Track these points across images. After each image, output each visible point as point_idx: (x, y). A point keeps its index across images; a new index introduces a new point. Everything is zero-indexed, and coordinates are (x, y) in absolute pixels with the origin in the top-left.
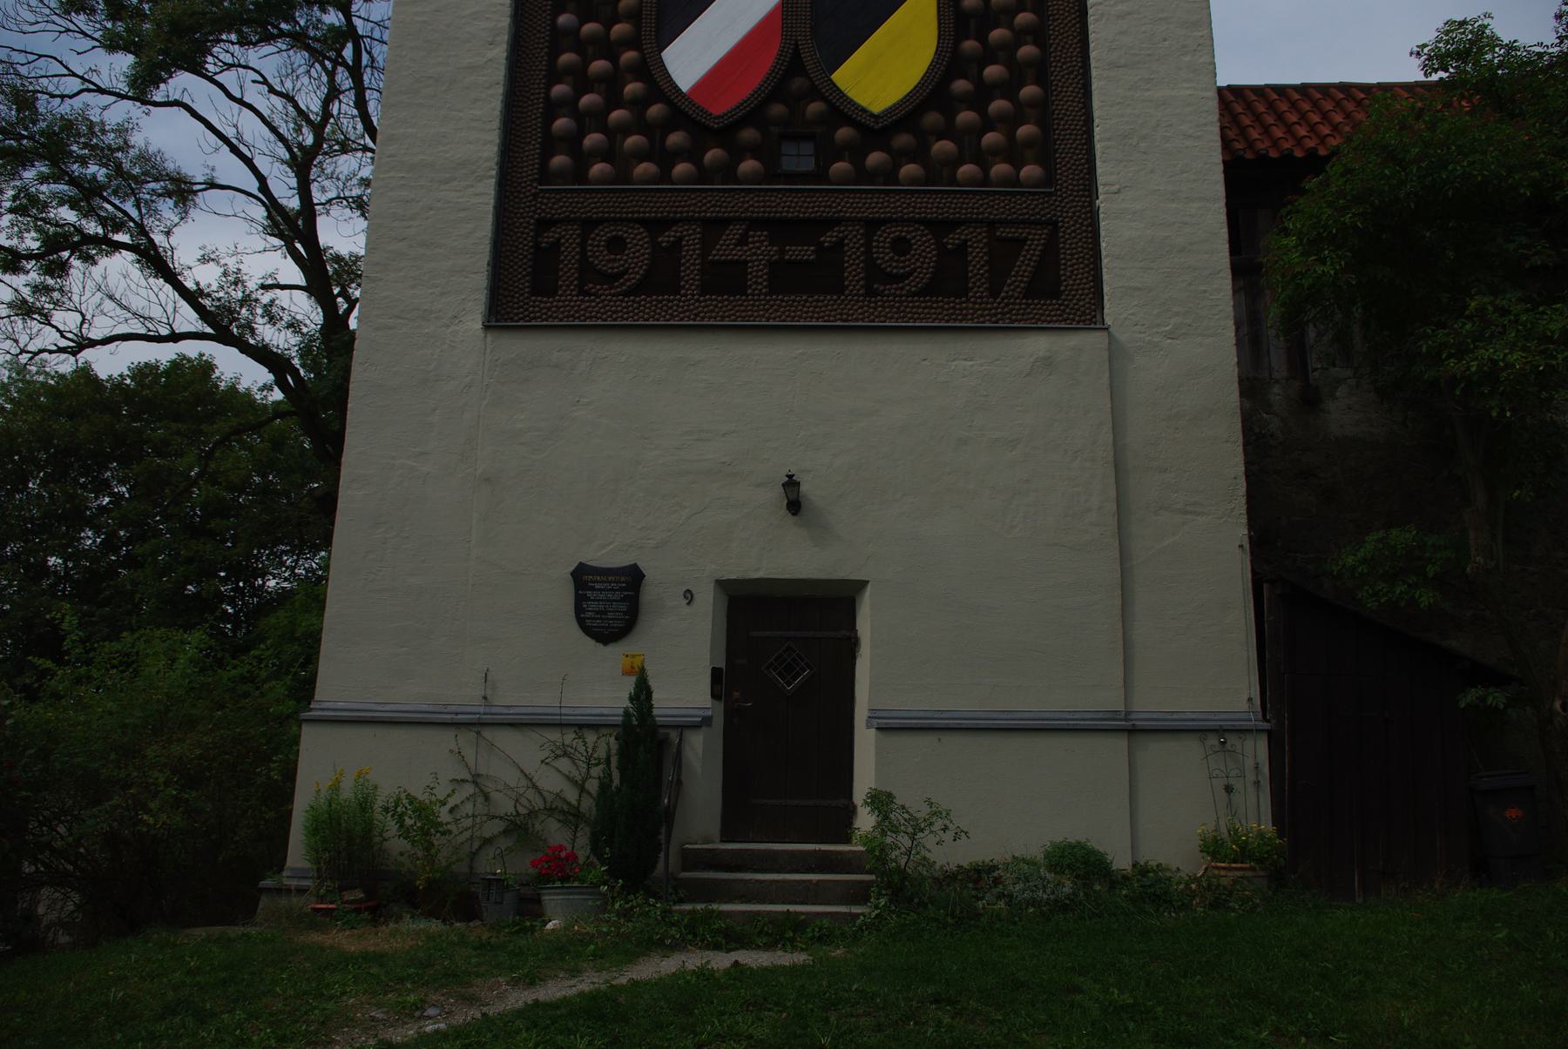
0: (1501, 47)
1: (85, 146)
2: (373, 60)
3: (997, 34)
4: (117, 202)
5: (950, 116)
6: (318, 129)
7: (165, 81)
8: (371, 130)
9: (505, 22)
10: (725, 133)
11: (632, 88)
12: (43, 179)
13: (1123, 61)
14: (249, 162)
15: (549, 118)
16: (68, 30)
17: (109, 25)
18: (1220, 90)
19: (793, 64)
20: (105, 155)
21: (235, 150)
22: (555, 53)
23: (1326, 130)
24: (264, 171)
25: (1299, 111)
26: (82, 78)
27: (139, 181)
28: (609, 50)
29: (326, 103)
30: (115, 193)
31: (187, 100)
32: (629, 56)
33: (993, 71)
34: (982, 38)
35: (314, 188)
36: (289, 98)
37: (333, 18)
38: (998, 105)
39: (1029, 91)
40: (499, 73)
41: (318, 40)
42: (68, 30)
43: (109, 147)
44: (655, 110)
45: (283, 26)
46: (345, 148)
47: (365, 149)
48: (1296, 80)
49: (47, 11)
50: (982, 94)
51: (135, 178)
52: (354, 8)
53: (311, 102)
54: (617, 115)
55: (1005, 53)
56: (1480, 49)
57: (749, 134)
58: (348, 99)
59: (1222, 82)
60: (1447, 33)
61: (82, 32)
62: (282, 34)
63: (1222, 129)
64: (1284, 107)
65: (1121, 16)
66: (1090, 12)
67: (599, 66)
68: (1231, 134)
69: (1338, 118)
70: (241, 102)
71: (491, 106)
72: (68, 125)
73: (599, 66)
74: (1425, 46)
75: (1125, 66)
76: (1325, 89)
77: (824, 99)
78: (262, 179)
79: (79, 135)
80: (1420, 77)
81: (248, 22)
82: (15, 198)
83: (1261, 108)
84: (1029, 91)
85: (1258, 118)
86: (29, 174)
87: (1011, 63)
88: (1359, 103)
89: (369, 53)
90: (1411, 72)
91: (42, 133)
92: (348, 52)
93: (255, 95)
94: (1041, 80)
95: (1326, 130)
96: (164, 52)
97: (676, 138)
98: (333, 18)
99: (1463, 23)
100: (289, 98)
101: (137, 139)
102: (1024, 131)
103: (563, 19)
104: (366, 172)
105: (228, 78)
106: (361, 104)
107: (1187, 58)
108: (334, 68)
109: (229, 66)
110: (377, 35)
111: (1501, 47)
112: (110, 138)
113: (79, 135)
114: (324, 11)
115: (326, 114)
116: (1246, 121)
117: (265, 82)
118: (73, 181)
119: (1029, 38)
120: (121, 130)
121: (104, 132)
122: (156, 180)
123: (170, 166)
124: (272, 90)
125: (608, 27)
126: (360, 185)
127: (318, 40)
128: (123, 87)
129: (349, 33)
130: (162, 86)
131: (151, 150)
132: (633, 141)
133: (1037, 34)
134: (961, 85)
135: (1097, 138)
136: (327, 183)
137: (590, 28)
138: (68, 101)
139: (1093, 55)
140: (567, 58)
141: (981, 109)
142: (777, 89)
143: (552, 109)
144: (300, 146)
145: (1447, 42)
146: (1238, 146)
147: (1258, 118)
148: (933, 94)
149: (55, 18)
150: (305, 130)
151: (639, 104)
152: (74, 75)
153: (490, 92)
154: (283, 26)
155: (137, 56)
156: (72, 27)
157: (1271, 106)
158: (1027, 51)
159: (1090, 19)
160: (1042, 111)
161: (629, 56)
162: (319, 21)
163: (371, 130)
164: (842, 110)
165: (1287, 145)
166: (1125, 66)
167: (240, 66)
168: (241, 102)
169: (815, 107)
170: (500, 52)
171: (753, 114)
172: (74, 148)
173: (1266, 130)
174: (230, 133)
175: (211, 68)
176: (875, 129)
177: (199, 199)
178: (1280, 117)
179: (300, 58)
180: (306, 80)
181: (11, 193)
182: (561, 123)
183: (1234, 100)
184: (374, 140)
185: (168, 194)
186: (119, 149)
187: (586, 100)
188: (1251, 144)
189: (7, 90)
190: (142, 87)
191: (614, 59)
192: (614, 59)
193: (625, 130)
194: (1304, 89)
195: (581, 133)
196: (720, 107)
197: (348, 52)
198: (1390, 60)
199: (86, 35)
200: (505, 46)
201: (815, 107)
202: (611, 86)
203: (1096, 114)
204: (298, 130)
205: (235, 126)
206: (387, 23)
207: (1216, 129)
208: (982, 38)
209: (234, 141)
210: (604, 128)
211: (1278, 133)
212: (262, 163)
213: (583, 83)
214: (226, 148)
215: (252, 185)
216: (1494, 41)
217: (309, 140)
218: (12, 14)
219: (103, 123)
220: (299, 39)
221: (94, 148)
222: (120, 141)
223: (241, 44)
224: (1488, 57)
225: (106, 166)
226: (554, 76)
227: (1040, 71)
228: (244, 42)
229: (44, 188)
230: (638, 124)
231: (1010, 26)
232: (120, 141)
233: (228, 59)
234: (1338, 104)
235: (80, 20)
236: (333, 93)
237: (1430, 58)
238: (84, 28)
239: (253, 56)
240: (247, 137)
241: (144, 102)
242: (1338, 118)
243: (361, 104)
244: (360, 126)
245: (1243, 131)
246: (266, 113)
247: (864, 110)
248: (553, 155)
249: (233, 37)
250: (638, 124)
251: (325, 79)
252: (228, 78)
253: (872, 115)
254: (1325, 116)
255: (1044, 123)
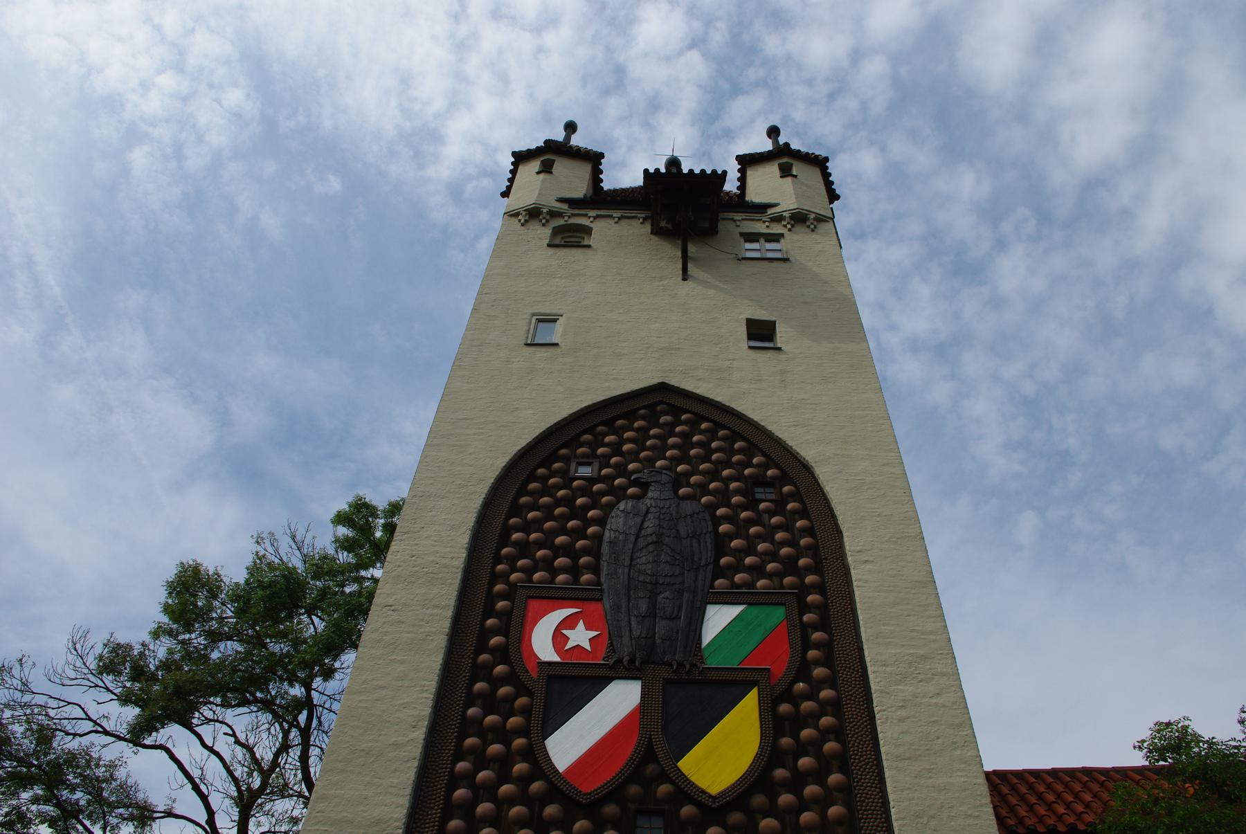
0: (1204, 742)
1: (81, 775)
2: (320, 723)
3: (806, 733)
4: (87, 823)
5: (773, 798)
6: (266, 775)
7: (157, 730)
8: (310, 785)
9: (427, 711)
10: (591, 808)
11: (520, 767)
12: (36, 800)
13: (907, 755)
14: (204, 798)
15: (451, 788)
16: (97, 686)
17: (128, 684)
18: (990, 776)
19: (648, 754)
20: (94, 787)
21: (196, 788)
22: (462, 736)
23: (1080, 808)
24: (214, 807)
25: (1054, 791)
26: (95, 722)
27: (113, 806)
28: (504, 735)
29: (277, 755)
30: (89, 817)
31: (169, 745)
32: (519, 742)
33: (805, 762)
34: (795, 736)
35: (252, 822)
36: (249, 749)
37: (297, 691)
38: (811, 790)
39: (834, 778)
40: (417, 750)
41: (282, 707)
42: (97, 686)
43: (97, 779)
44: (536, 786)
45: (258, 695)
46: (283, 791)
47: (300, 795)
48: (1048, 766)
49: (86, 671)
50: (797, 782)
51: (110, 804)
52: (314, 685)
53: (265, 753)
54: (505, 788)
55: (813, 747)
56: (1188, 744)
57: (610, 809)
58: (295, 753)
59: (988, 767)
60: (1158, 731)
61: (108, 689)
62: (256, 701)
63: (994, 808)
64: (1042, 789)
65: (902, 720)
66: (877, 716)
67: (495, 748)
68: (1003, 812)
69: (1088, 798)
70: (211, 750)
71: (407, 776)
72: (71, 759)
73: (495, 748)
74: (1143, 741)
75: (909, 758)
76: (1072, 773)
77: (672, 782)
78: (211, 813)
79: (78, 767)
80: (1147, 763)
81: (234, 690)
82: (7, 814)
83: (1024, 789)
84: (834, 778)
85: (1022, 798)
86: (26, 795)
87: (819, 755)
88: (1102, 784)
89: (319, 718)
90: (1138, 759)
91: (49, 763)
92: (302, 718)
93: (224, 745)
94: (844, 769)
95: (1080, 808)
96: (163, 708)
97: (551, 810)
98: (297, 691)
99: (1169, 724)
100: (249, 749)
101: (121, 774)
102: (834, 811)
103: (471, 711)
104: (296, 813)
105: (206, 731)
106: (304, 758)
107: (958, 752)
108: (290, 728)
109: (208, 721)
110: (327, 705)
111: (1204, 742)
112: (100, 772)
113: (78, 767)
114: (292, 685)
115: (275, 764)
116: (1014, 800)
117: (234, 735)
118: (59, 805)
119: (832, 736)
120: (112, 766)
121: (98, 766)
122: (126, 806)
123: (141, 796)
124: (237, 742)
125: (506, 719)
126: (289, 822)
127: (282, 707)
128: (123, 730)
129: (307, 703)
130: (154, 734)
131: (130, 782)
132: (516, 810)
133: (837, 732)
134: (780, 773)
135: (893, 817)
136: (263, 819)
137: (490, 719)
138: (78, 738)
139: (883, 750)
140: (470, 741)
141: (798, 792)
142: (635, 773)
143: (455, 781)
144: (249, 788)
145: (1160, 739)
146: (1011, 822)
147: (1022, 798)
148: (758, 780)
149: (90, 677)
150: (255, 774)
151: (524, 780)
152: (90, 719)
153: (409, 764)
154: (258, 695)
155: (143, 710)
156: (101, 683)
157: (1031, 787)
158: (830, 746)
159: (878, 722)
160: (846, 793)
161: (519, 742)
162: (286, 693)
163: (310, 785)
164: (686, 791)
165: (1051, 822)
166: (909, 758)
167: (217, 721)
168: (211, 750)
169: (664, 788)
170: (420, 734)
171: (615, 793)
172: (70, 777)
173: (1031, 808)
174: (195, 773)
175: (195, 721)
176: (714, 808)
177: (155, 825)
178: (1040, 796)
179: (265, 718)
180: (265, 735)
181: (6, 810)
182: (460, 793)
183: (1000, 782)
184: (310, 791)
185: (131, 818)
186: (106, 781)
187: (482, 775)
188: (1021, 820)
189: (35, 727)
190: (137, 736)
191: (507, 744)
192: (507, 744)
193: (511, 801)
194: (1055, 773)
195: (475, 802)
196: (590, 786)
197: (302, 718)
198: (1118, 747)
199: (108, 689)
200: (424, 729)
201: (664, 788)
202: (503, 766)
203: (891, 797)
204: (250, 774)
205: (202, 769)
206: (337, 697)
207: (991, 810)
208: (795, 736)
209: (197, 780)
210: (494, 798)
211: (1042, 810)
212: (214, 800)
213: (481, 761)
214: (190, 786)
215: (202, 817)
216: (1197, 738)
217: (256, 783)
218: (60, 671)
219: (100, 759)
220: (267, 705)
221: (85, 778)
222: (108, 774)
223: (222, 706)
224: (1196, 750)
225: (90, 793)
226: (459, 755)
227: (842, 762)
228: (226, 705)
229: (34, 808)
230: (523, 797)
231: (816, 727)
232: (108, 774)
233: (209, 714)
234: (1085, 785)
235: (108, 679)
236: (284, 748)
237: (1150, 751)
238: (109, 685)
239: (229, 715)
240: (209, 777)
241: (136, 744)
242: (1088, 798)
243: (304, 758)
244: (300, 776)
245: (1012, 809)
246: (228, 759)
247: (704, 792)
248: (451, 819)
249: (218, 700)
250: (523, 797)
251: (281, 735)
252: (206, 731)
253: (710, 796)
254: (1076, 795)
255: (849, 804)
